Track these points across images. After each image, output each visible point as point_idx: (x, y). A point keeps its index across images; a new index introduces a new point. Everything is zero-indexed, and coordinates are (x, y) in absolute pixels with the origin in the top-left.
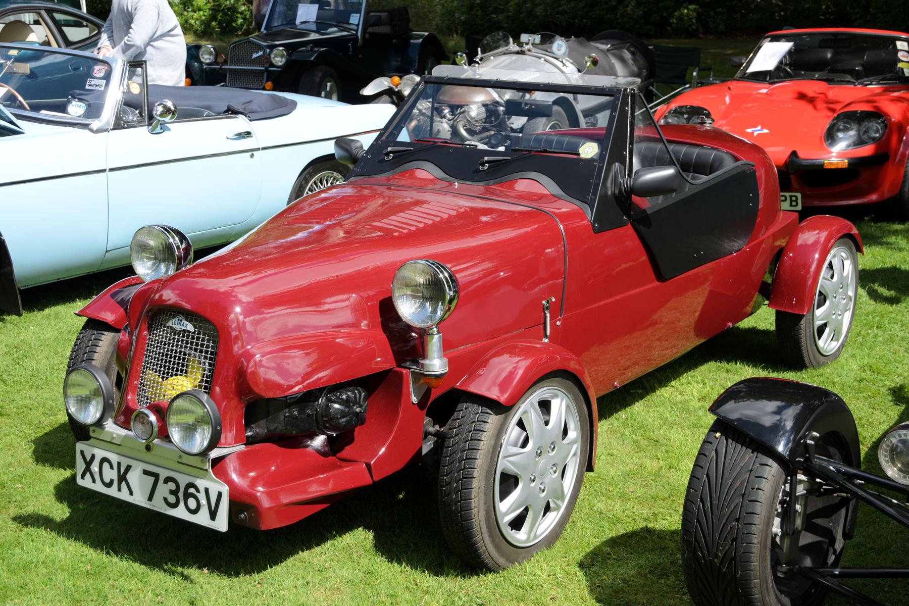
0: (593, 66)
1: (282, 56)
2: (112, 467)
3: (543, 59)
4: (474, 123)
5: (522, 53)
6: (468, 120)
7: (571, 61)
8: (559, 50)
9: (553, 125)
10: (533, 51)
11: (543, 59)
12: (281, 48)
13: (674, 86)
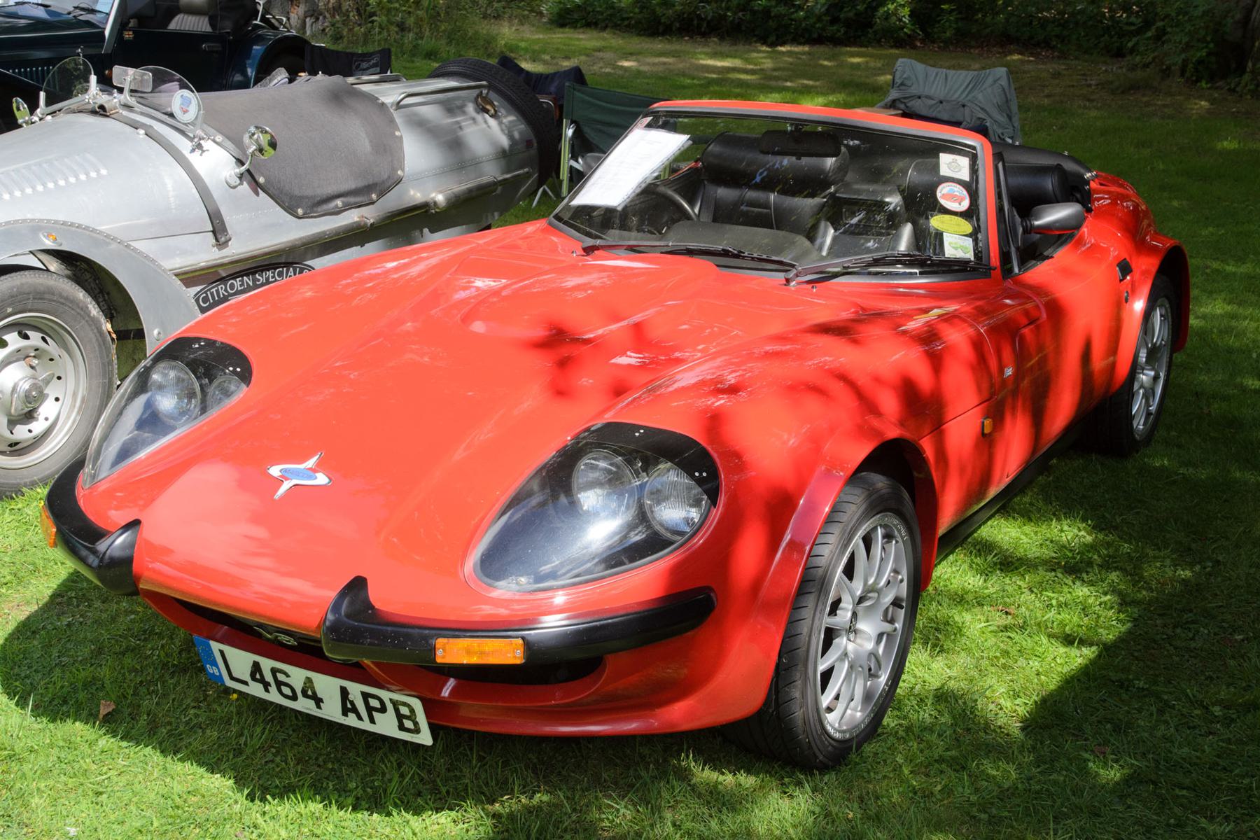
8: (185, 112)
11: (142, 132)
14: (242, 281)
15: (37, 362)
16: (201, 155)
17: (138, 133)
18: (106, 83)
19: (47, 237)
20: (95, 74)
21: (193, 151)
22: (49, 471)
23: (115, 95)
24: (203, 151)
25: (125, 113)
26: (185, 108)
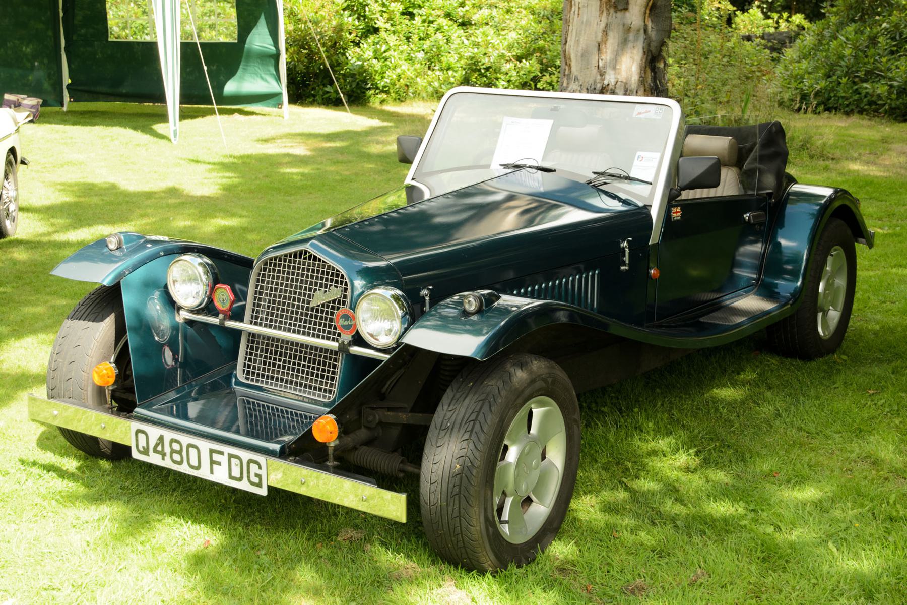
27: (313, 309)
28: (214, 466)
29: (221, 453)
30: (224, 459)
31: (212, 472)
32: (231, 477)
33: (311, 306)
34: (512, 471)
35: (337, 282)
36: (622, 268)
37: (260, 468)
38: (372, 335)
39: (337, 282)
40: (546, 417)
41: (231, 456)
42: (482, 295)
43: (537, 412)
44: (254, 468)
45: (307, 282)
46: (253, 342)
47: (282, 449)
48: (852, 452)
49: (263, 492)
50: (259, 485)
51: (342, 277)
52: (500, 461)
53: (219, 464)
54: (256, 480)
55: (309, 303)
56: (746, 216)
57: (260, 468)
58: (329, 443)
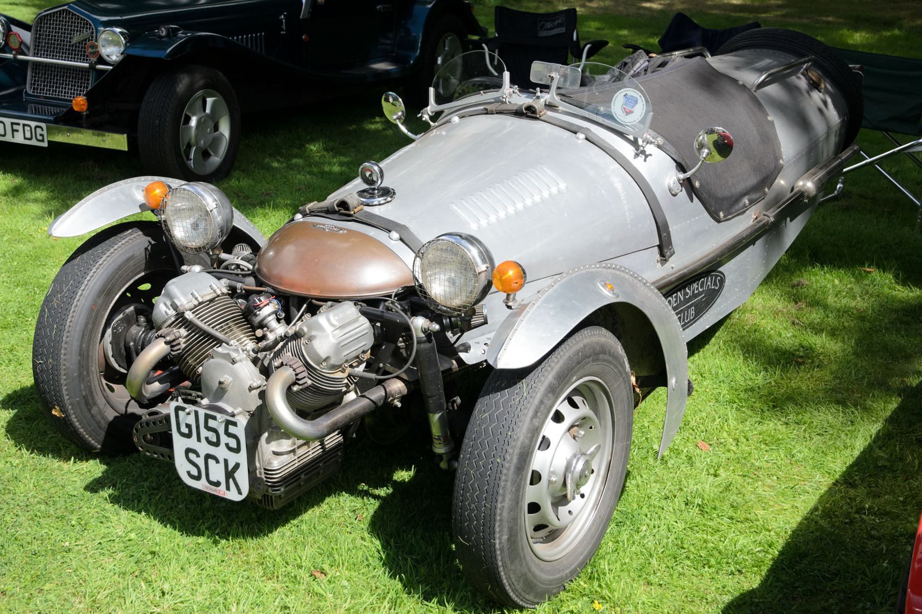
0: (718, 158)
1: (116, 43)
2: (218, 462)
3: (581, 136)
4: (326, 372)
5: (529, 113)
6: (307, 365)
7: (660, 140)
8: (628, 113)
9: (584, 385)
10: (560, 108)
11: (581, 136)
12: (118, 30)
13: (899, 137)
14: (676, 297)
15: (583, 433)
16: (645, 161)
17: (578, 138)
18: (523, 83)
19: (605, 286)
20: (507, 71)
21: (637, 155)
22: (582, 557)
23: (539, 94)
24: (646, 156)
25: (549, 113)
26: (628, 108)
27: (73, 46)
28: (15, 133)
29: (19, 124)
30: (20, 128)
31: (13, 137)
32: (25, 138)
33: (72, 44)
34: (193, 130)
35: (87, 28)
36: (282, 32)
37: (42, 130)
38: (108, 56)
39: (87, 28)
40: (214, 104)
41: (24, 125)
42: (171, 28)
43: (210, 101)
44: (39, 130)
45: (68, 29)
46: (36, 69)
47: (55, 119)
48: (795, 383)
49: (45, 144)
50: (43, 141)
51: (90, 25)
52: (184, 124)
53: (17, 131)
54: (40, 138)
55: (70, 42)
56: (378, 7)
57: (42, 130)
58: (83, 112)
